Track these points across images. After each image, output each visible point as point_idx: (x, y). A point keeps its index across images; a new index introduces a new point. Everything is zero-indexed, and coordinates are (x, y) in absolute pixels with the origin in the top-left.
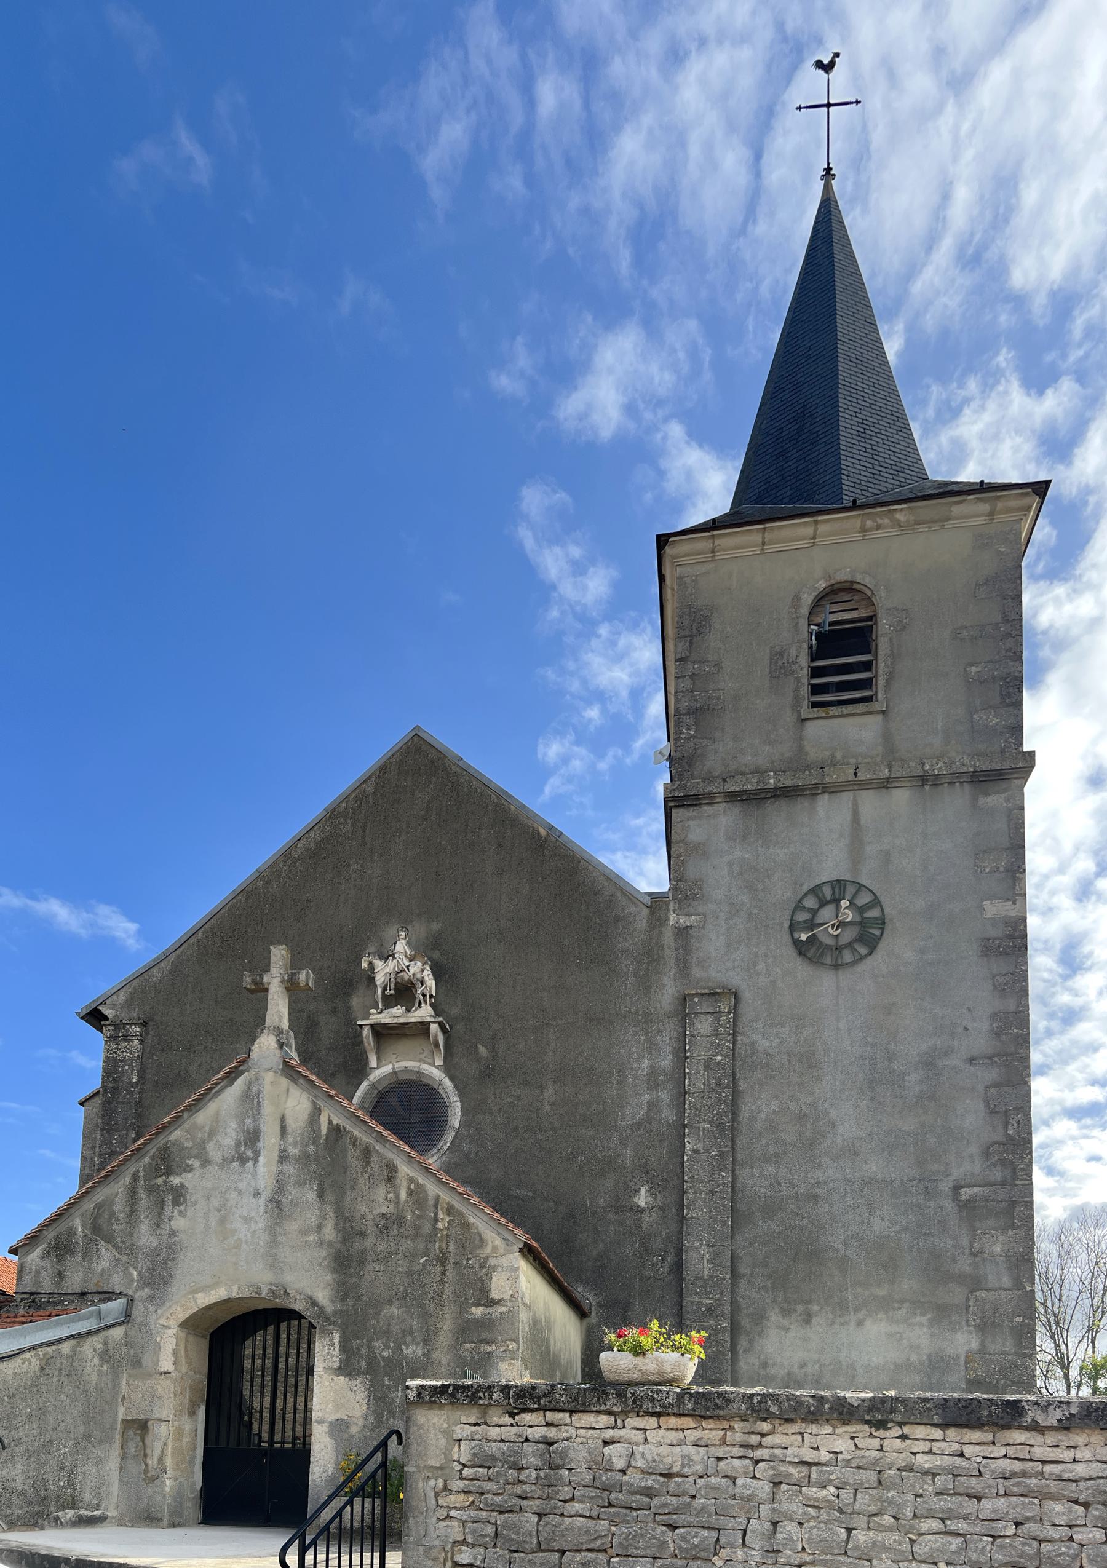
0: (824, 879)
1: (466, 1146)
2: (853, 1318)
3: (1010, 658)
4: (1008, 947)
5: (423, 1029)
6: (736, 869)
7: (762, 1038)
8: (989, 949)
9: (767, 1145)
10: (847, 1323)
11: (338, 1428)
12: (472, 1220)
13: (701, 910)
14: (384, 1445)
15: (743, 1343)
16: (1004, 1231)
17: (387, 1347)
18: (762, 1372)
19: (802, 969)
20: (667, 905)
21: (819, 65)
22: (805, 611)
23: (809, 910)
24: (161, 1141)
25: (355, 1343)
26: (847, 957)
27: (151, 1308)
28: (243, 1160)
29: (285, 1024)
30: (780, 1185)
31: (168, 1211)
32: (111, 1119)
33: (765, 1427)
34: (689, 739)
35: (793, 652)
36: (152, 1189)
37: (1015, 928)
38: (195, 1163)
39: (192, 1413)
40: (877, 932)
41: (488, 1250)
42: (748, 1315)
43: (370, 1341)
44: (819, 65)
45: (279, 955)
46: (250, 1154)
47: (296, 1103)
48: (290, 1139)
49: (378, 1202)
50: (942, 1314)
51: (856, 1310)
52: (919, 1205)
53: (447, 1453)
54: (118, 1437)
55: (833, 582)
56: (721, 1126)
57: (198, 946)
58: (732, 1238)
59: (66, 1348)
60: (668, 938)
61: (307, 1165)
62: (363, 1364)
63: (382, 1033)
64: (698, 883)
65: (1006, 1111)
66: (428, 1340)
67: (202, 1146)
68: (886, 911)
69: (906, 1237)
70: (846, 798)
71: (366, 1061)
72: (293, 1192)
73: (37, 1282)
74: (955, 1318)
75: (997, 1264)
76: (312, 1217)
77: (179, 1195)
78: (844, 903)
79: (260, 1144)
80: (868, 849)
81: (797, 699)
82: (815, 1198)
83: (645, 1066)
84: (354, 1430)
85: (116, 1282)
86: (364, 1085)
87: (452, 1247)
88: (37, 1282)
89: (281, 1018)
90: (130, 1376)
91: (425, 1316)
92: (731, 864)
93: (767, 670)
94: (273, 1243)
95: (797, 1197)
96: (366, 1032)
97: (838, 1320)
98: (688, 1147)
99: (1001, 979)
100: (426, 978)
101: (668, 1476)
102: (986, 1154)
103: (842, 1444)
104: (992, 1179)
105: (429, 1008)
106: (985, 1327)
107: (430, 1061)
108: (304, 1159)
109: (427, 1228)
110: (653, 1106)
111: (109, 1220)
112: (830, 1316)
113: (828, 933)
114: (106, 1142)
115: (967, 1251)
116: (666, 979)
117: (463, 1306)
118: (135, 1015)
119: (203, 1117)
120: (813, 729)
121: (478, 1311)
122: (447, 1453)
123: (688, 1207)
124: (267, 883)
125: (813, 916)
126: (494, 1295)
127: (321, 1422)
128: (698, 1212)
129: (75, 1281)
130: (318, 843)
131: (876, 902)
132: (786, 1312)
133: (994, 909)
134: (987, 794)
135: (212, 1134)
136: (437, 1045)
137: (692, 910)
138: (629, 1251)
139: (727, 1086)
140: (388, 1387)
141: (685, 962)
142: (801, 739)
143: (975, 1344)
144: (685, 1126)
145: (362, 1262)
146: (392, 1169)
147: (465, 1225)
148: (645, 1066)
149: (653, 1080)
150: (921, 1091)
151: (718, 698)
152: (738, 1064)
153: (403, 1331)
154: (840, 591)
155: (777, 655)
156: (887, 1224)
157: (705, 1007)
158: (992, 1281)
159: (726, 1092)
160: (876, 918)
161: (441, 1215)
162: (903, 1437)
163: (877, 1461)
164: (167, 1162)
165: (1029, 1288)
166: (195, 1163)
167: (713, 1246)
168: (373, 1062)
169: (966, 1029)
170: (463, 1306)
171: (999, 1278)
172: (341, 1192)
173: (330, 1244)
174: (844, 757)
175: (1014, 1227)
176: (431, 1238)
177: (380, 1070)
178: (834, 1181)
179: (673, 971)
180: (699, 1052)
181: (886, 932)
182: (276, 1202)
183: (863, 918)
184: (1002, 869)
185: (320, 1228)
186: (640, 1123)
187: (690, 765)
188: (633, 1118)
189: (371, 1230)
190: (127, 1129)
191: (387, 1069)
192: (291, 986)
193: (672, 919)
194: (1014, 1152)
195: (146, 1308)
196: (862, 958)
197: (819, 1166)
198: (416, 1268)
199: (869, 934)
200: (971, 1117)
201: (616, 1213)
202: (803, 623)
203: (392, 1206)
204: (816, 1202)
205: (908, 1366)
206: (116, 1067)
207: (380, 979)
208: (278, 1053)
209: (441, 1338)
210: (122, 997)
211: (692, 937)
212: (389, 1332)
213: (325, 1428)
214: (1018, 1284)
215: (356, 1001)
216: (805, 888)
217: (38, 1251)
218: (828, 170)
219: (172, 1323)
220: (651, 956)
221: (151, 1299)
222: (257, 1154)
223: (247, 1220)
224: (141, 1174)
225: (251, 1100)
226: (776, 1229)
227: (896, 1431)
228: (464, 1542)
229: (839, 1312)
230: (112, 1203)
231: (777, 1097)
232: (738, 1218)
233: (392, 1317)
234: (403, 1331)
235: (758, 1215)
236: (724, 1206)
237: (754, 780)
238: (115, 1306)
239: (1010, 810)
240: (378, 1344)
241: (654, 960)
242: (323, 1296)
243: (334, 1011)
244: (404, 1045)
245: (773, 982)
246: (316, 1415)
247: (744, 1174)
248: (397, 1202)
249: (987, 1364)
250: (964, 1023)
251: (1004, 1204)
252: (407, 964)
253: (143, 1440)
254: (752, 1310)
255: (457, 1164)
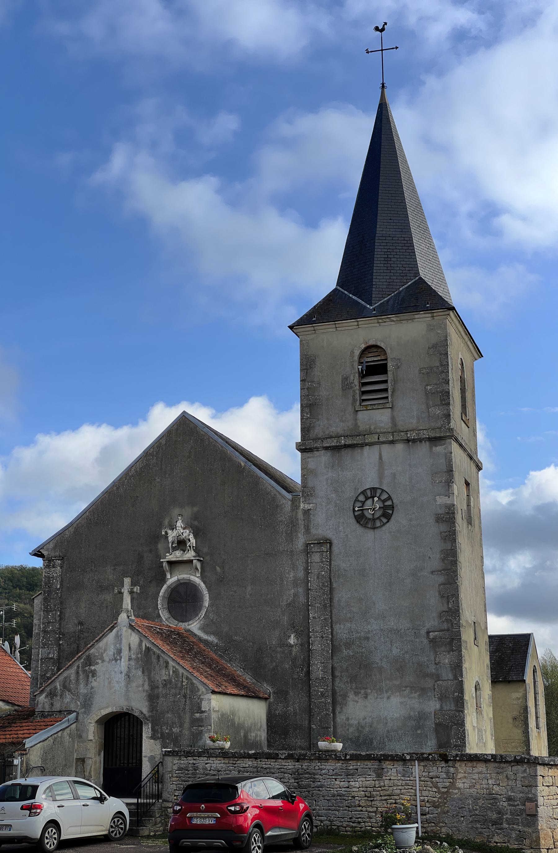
0: (368, 487)
1: (211, 616)
2: (386, 695)
3: (444, 382)
4: (447, 518)
5: (190, 562)
6: (329, 481)
7: (341, 562)
8: (439, 519)
9: (346, 613)
10: (383, 698)
11: (152, 758)
12: (195, 682)
13: (314, 502)
14: (158, 766)
15: (338, 709)
16: (449, 652)
17: (167, 729)
18: (347, 723)
19: (359, 530)
20: (299, 499)
21: (377, 29)
22: (356, 358)
23: (361, 501)
24: (87, 653)
25: (156, 728)
26: (378, 524)
27: (85, 716)
28: (116, 660)
29: (130, 607)
30: (352, 632)
31: (90, 680)
32: (48, 605)
33: (236, 759)
34: (307, 419)
35: (352, 378)
36: (84, 671)
37: (449, 509)
38: (100, 661)
39: (99, 755)
40: (390, 512)
41: (200, 693)
42: (340, 695)
43: (161, 727)
44: (377, 29)
45: (127, 581)
46: (118, 658)
47: (134, 639)
48: (132, 652)
49: (162, 675)
50: (423, 691)
51: (387, 692)
52: (412, 641)
53: (172, 767)
54: (74, 765)
55: (368, 345)
56: (325, 606)
57: (87, 519)
58: (332, 658)
59: (60, 734)
60: (300, 515)
61: (138, 662)
62: (159, 735)
63: (171, 563)
64: (313, 488)
65: (448, 596)
66: (181, 726)
67: (102, 655)
68: (394, 502)
69: (407, 656)
70: (376, 447)
71: (166, 575)
72: (134, 671)
73: (43, 707)
74: (429, 694)
75: (446, 668)
76: (140, 682)
77: (94, 673)
78: (376, 499)
79: (122, 654)
80: (386, 472)
81: (354, 400)
82: (368, 638)
83: (291, 576)
84: (157, 759)
85: (72, 707)
86: (165, 587)
87: (188, 692)
88: (43, 707)
89: (128, 605)
90: (78, 742)
91: (180, 717)
92: (327, 479)
93: (341, 386)
94: (127, 691)
95: (360, 638)
96: (164, 564)
97: (379, 697)
98: (311, 615)
99: (444, 534)
100: (191, 539)
101: (219, 771)
102: (440, 617)
103: (250, 763)
104: (443, 628)
105: (193, 551)
106: (442, 698)
107: (194, 574)
108: (137, 659)
109: (179, 685)
110: (295, 595)
111: (69, 683)
112: (376, 695)
113: (369, 514)
114: (46, 617)
115: (433, 662)
116: (300, 535)
117: (193, 713)
118: (58, 554)
119: (101, 644)
120: (361, 415)
121: (198, 715)
122: (172, 767)
123: (312, 644)
124: (118, 488)
125: (363, 504)
126: (203, 709)
127: (145, 757)
128: (316, 647)
129: (57, 706)
130: (141, 469)
131: (390, 498)
132: (356, 694)
133: (441, 500)
134: (436, 446)
135: (105, 650)
136: (197, 569)
137: (310, 501)
138: (287, 666)
139: (327, 586)
140: (168, 743)
141: (308, 526)
142: (356, 420)
143: (438, 707)
144: (310, 605)
145: (158, 698)
146: (167, 663)
147: (192, 684)
148: (291, 576)
149: (295, 584)
150: (411, 587)
151: (319, 399)
152: (332, 575)
153: (173, 723)
154: (369, 349)
155: (345, 379)
156: (399, 650)
157: (316, 549)
158: (444, 676)
159: (327, 589)
160: (389, 505)
161: (184, 680)
162: (261, 761)
163: (256, 767)
164: (89, 661)
165: (460, 679)
166: (100, 661)
167: (323, 663)
168: (168, 576)
169: (430, 558)
170: (193, 713)
171: (447, 674)
172: (150, 671)
173: (147, 691)
174: (375, 428)
175: (453, 651)
176: (181, 689)
177: (172, 580)
178: (375, 630)
179: (303, 531)
180: (314, 570)
181: (395, 511)
182: (128, 676)
183: (384, 506)
184: (443, 481)
185: (143, 685)
186: (290, 604)
187: (308, 432)
188: (287, 601)
189: (161, 686)
190: (56, 610)
191: (175, 579)
192: (131, 592)
193: (302, 505)
194: (452, 616)
195: (83, 716)
196: (384, 524)
197: (369, 623)
198: (177, 700)
199: (387, 513)
200: (433, 600)
201: (281, 647)
202: (356, 364)
203: (167, 677)
204: (368, 641)
205: (410, 717)
206: (49, 581)
207: (170, 539)
208: (127, 619)
209: (185, 725)
210: (51, 546)
211: (311, 514)
212: (168, 723)
213: (147, 759)
214: (456, 678)
215: (160, 546)
216: (360, 491)
217: (44, 695)
218: (383, 84)
219: (93, 721)
220: (293, 524)
221: (85, 713)
222: (121, 658)
223: (118, 682)
224: (80, 665)
225: (118, 637)
226: (351, 654)
227: (259, 760)
228: (176, 790)
229: (379, 693)
230: (70, 677)
231: (350, 591)
232: (335, 649)
233: (169, 717)
234: (173, 723)
235: (343, 647)
236: (327, 643)
237: (335, 441)
238: (73, 715)
239: (446, 454)
240: (165, 728)
241: (294, 526)
242: (145, 711)
243: (151, 551)
244: (182, 567)
245: (347, 535)
246: (143, 754)
247: (336, 627)
248: (169, 675)
249: (444, 715)
250: (429, 555)
251: (448, 640)
252: (182, 531)
253: (83, 766)
254: (341, 693)
255: (207, 625)
